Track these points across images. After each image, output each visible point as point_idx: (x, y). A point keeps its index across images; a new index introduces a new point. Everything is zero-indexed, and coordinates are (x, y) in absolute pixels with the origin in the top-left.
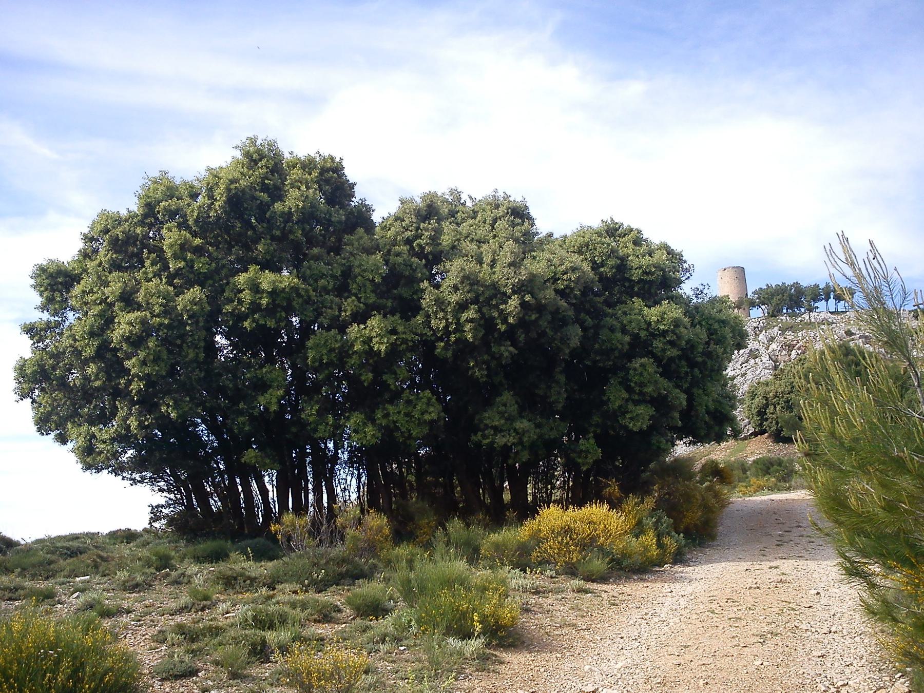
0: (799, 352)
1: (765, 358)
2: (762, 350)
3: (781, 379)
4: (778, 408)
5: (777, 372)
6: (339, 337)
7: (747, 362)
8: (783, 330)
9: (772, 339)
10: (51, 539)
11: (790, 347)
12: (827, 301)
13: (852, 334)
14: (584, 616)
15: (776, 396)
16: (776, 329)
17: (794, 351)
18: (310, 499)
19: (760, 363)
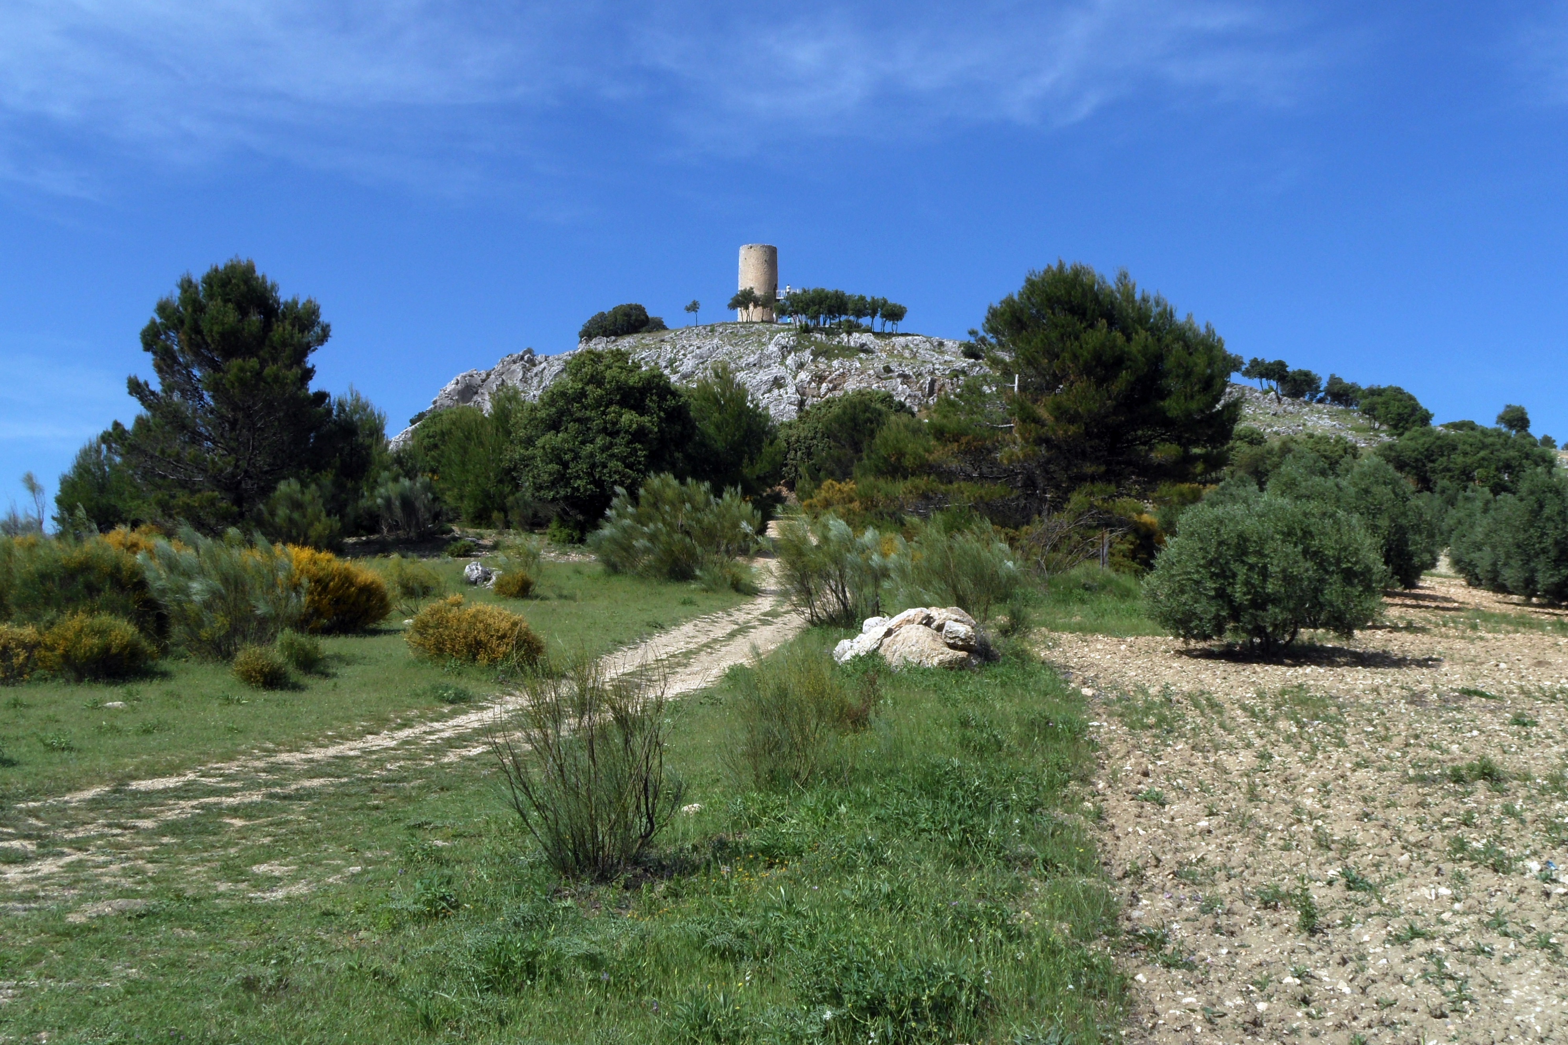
0: (831, 386)
1: (791, 389)
2: (789, 379)
3: (805, 423)
4: (799, 453)
5: (802, 414)
6: (1227, 1031)
7: (770, 391)
8: (816, 355)
9: (801, 366)
10: (382, 552)
11: (820, 379)
12: (873, 317)
13: (891, 371)
14: (799, 709)
15: (798, 441)
16: (808, 352)
17: (824, 385)
18: (293, 550)
19: (785, 396)
